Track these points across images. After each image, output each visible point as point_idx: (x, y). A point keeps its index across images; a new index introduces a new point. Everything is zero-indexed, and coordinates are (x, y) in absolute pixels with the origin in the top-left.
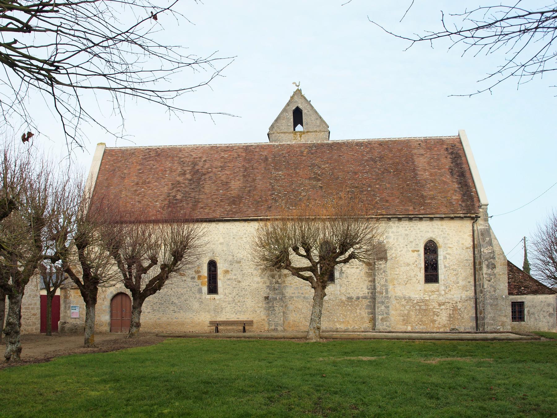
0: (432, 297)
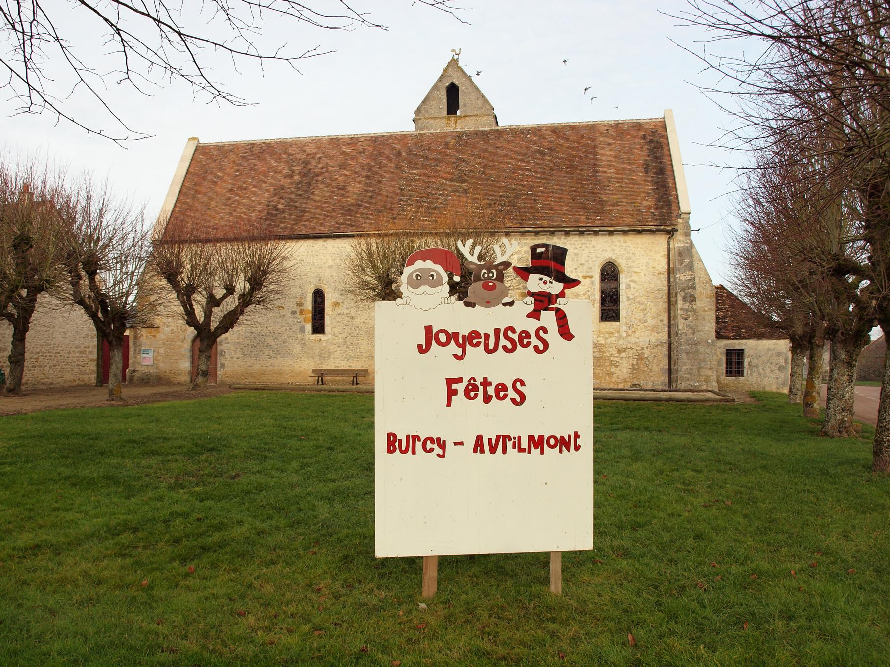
0: (608, 341)
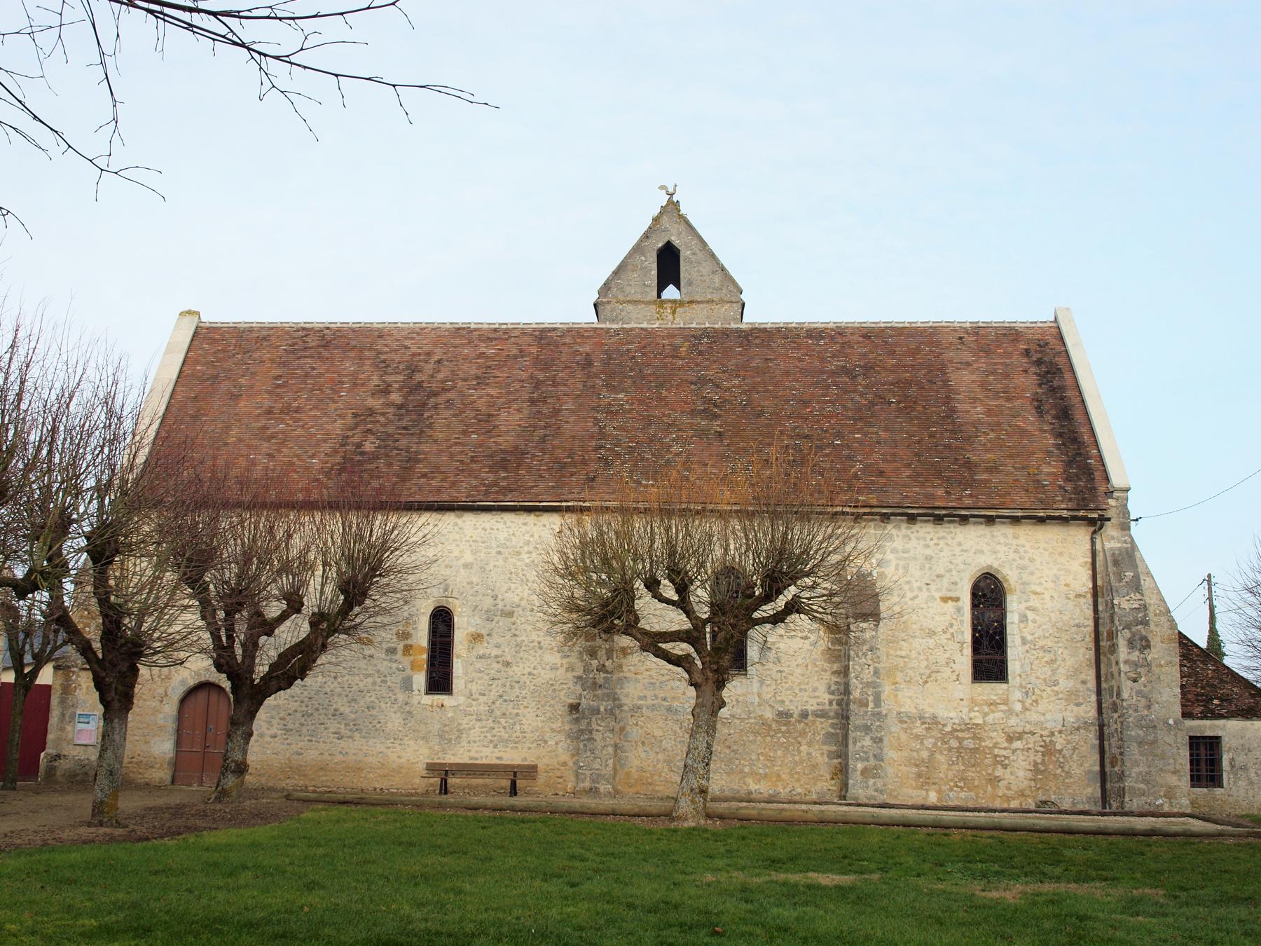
0: (990, 718)
